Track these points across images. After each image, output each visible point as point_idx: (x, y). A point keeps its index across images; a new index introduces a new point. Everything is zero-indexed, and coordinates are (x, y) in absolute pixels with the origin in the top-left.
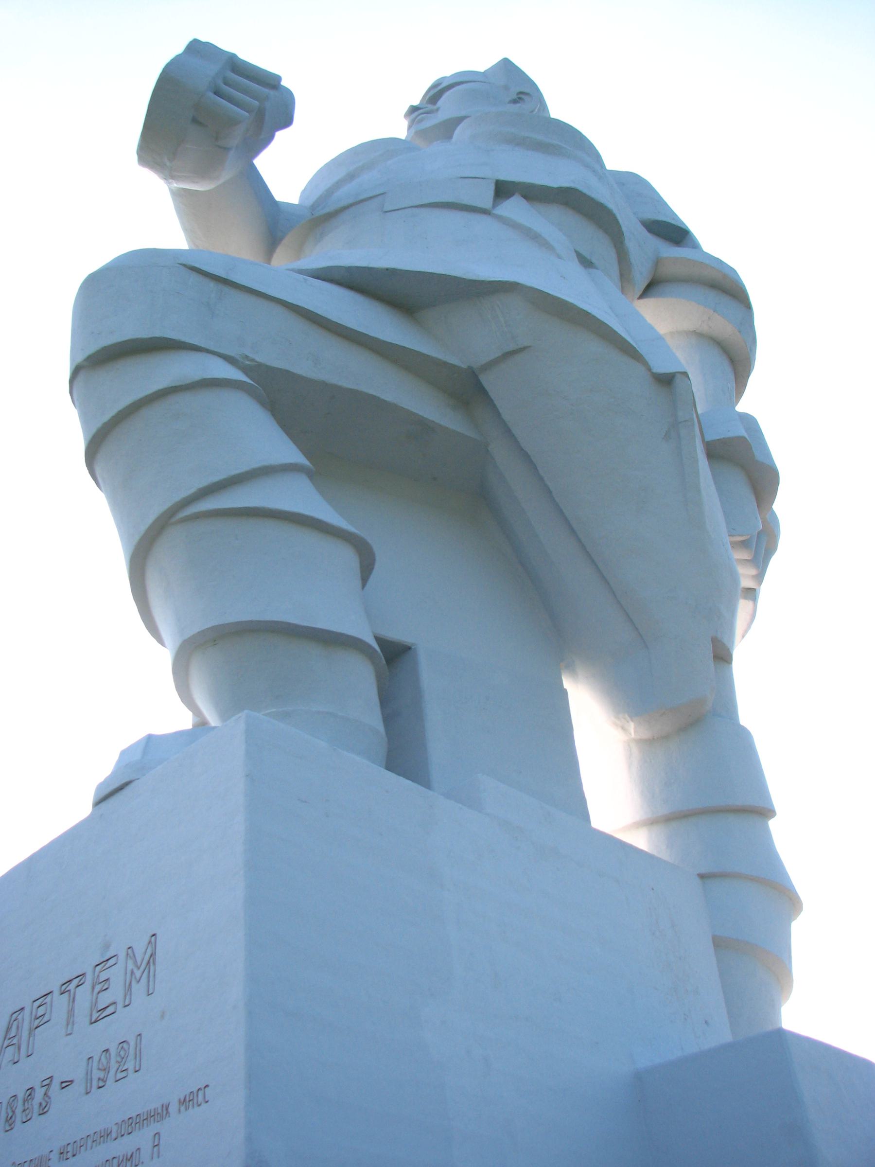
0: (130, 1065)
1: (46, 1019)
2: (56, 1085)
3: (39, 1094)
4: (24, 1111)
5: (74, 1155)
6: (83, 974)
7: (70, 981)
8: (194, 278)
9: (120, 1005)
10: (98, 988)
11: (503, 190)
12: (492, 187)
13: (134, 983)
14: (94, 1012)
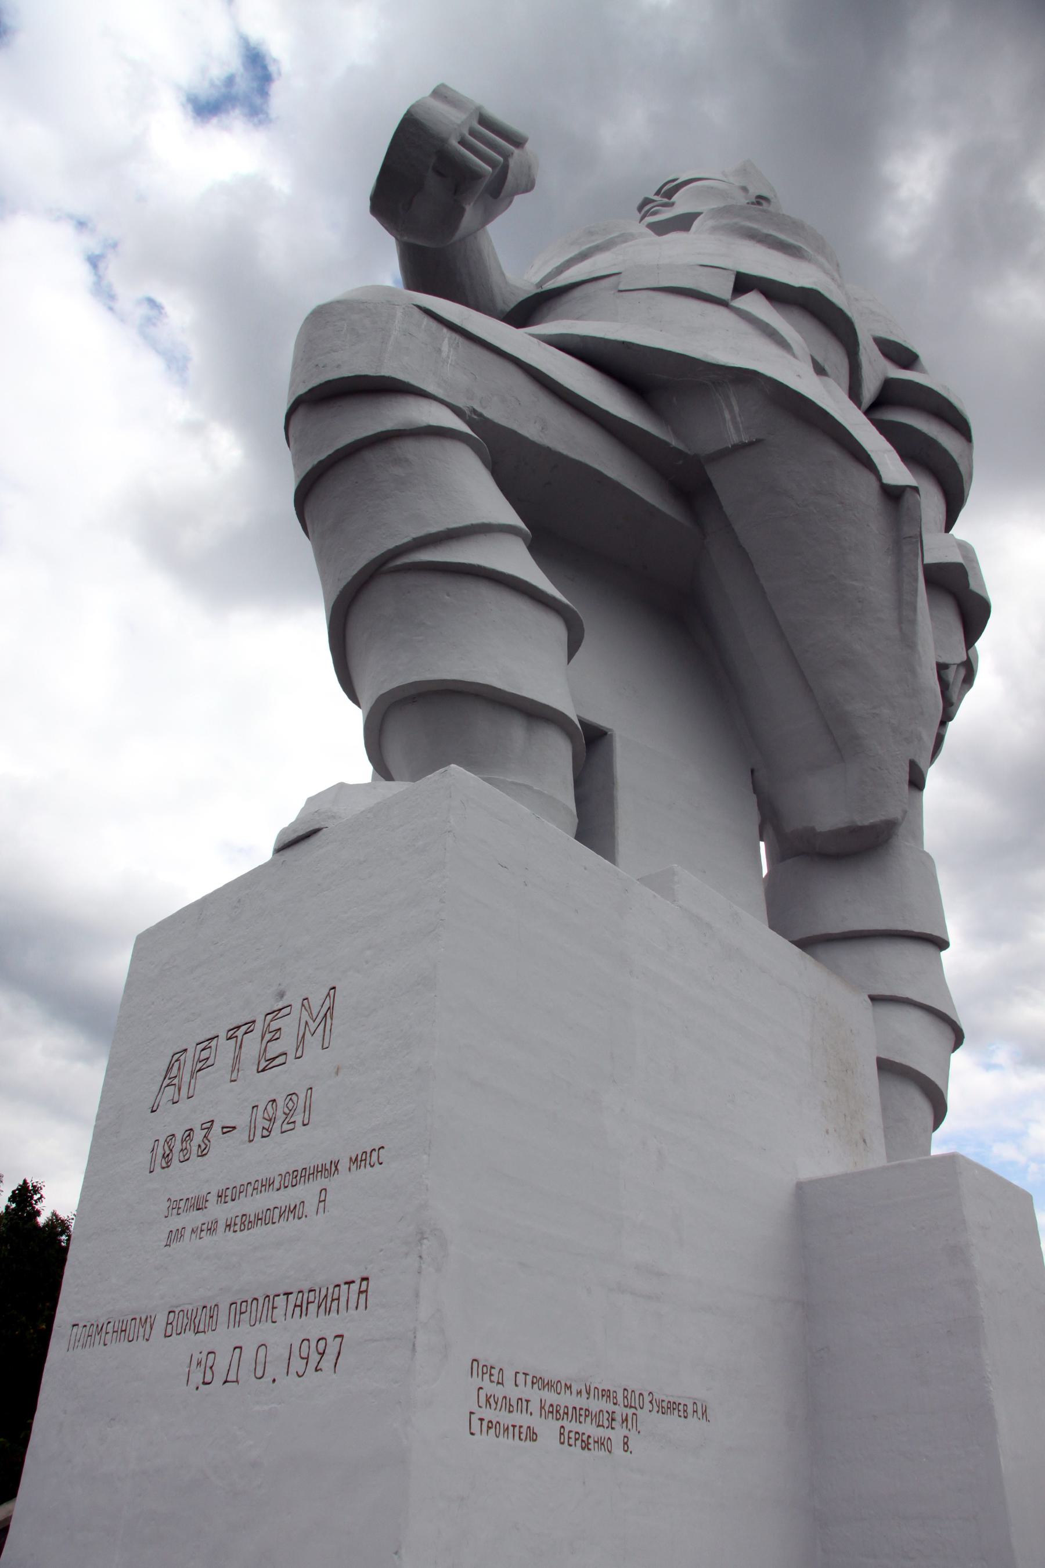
0: (298, 1118)
1: (209, 1062)
2: (217, 1129)
3: (199, 1136)
4: (182, 1150)
5: (233, 1200)
6: (254, 1022)
7: (239, 1027)
8: (426, 321)
9: (291, 1056)
10: (268, 1036)
11: (743, 284)
12: (733, 278)
13: (308, 1034)
14: (263, 1060)
